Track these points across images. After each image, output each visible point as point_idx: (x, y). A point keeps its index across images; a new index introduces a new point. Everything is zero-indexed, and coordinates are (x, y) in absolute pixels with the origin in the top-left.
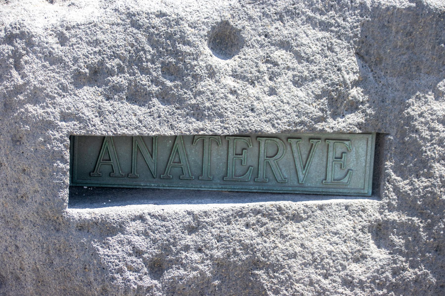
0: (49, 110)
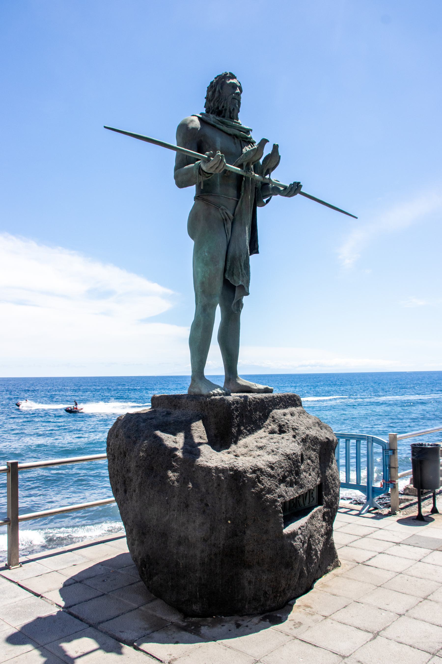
0: (274, 495)
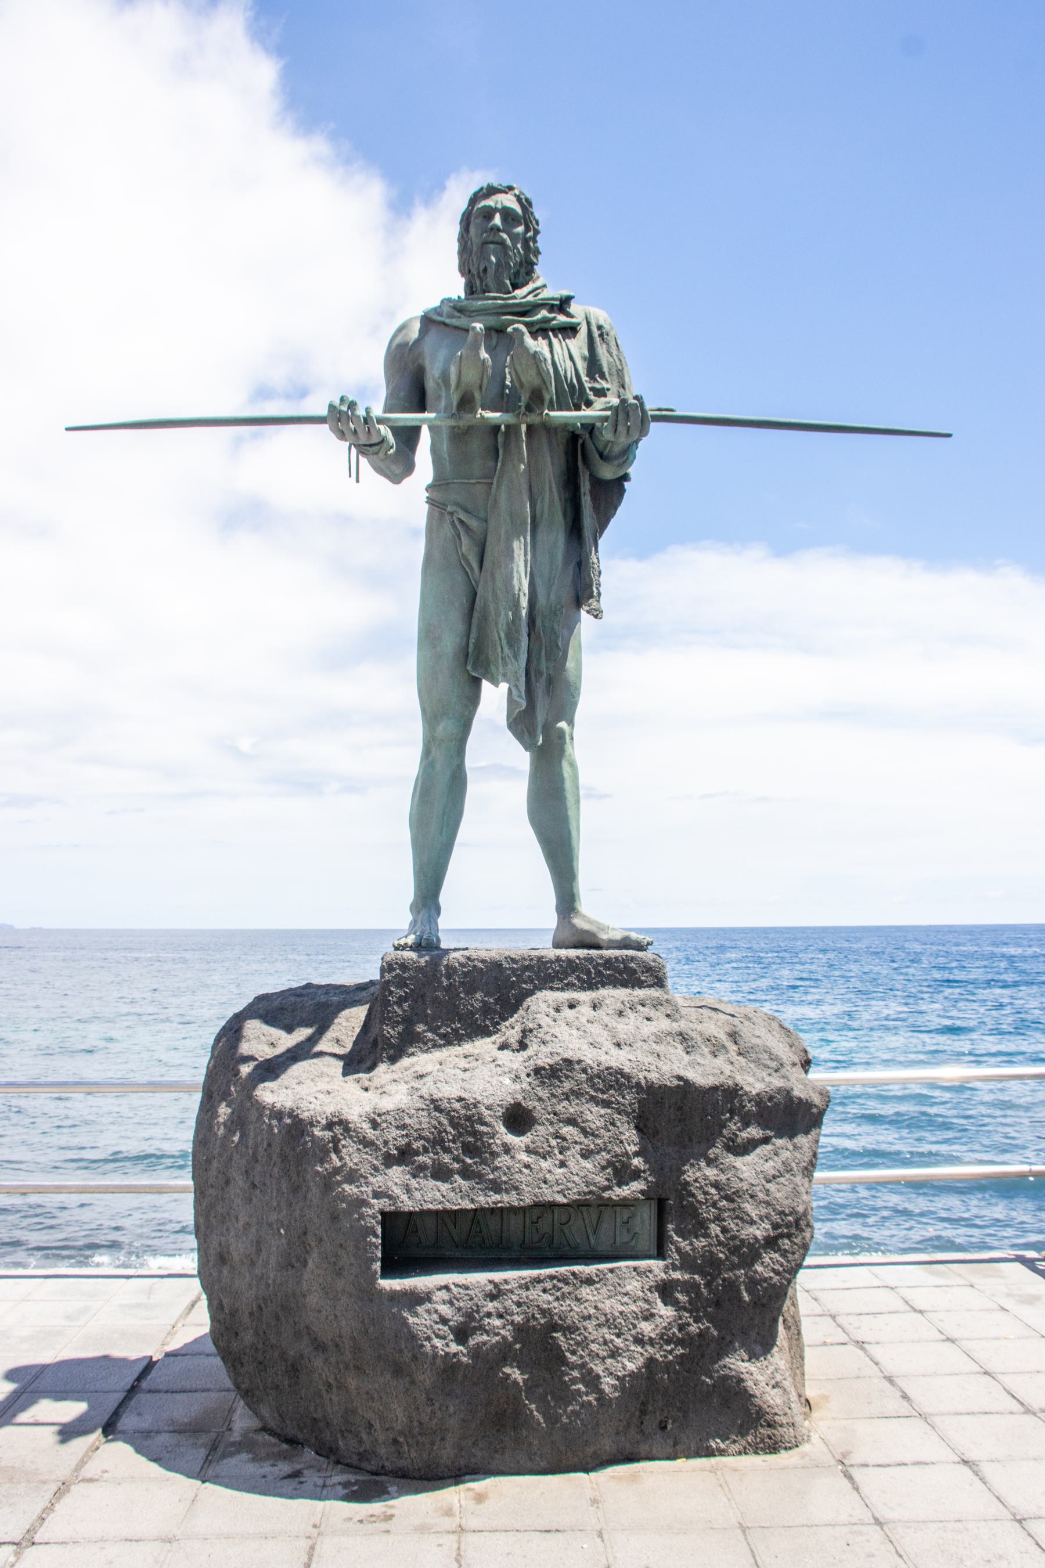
0: (363, 1189)
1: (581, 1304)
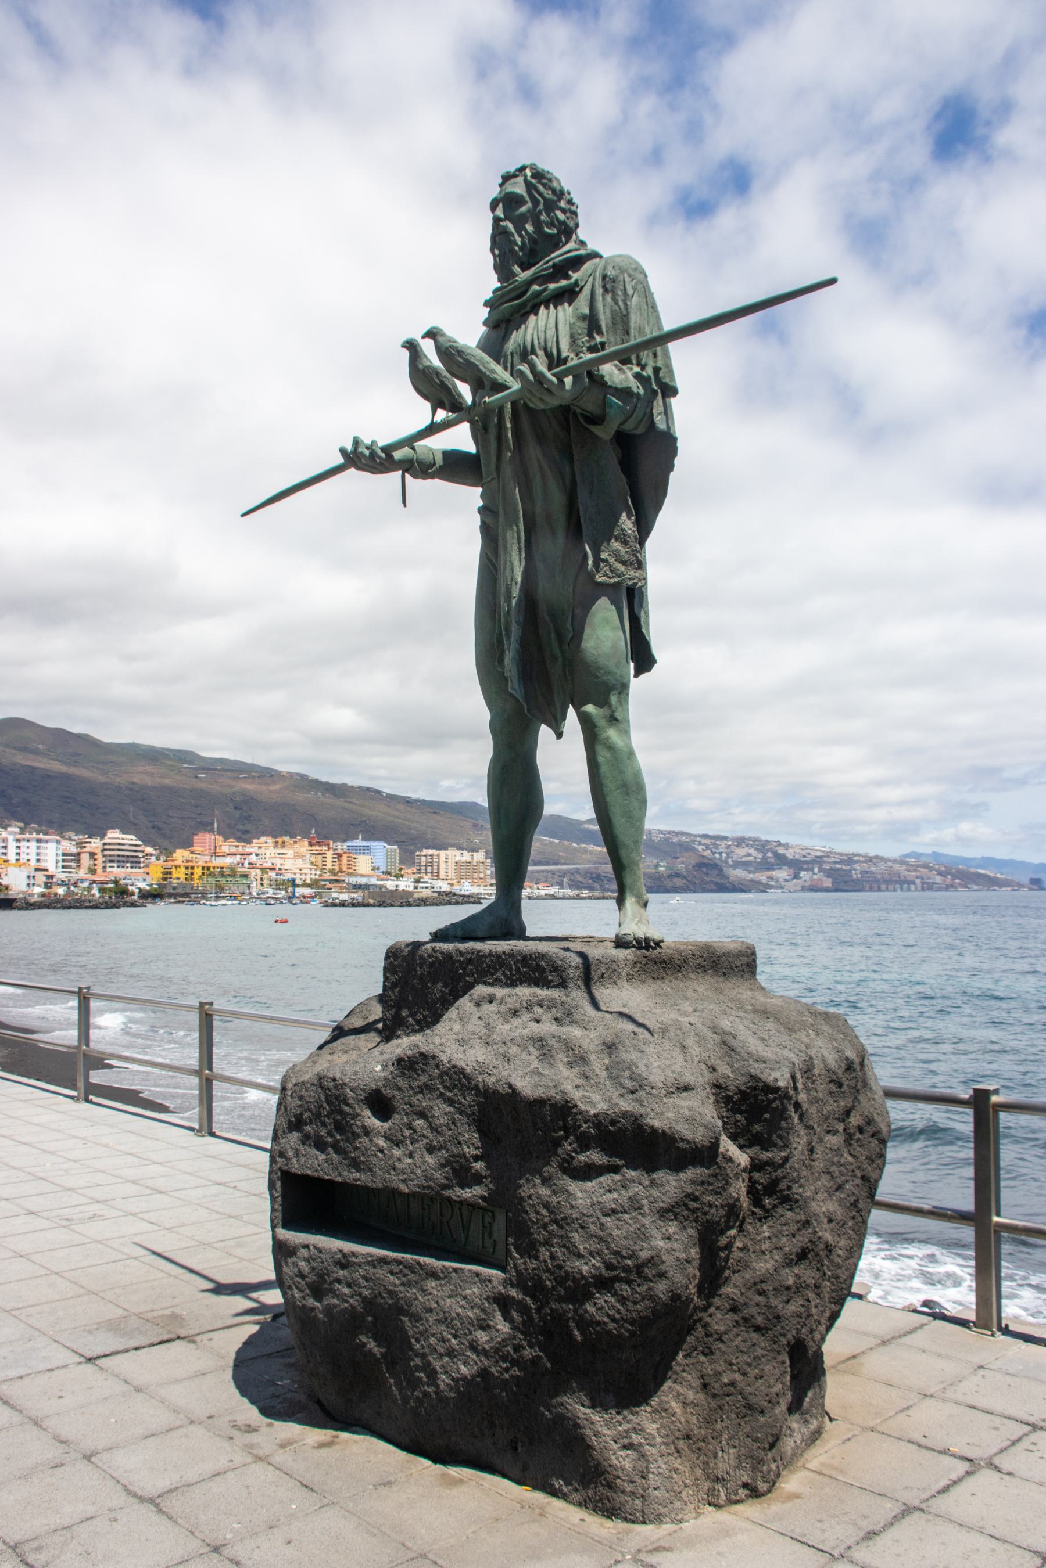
1: (426, 1295)
